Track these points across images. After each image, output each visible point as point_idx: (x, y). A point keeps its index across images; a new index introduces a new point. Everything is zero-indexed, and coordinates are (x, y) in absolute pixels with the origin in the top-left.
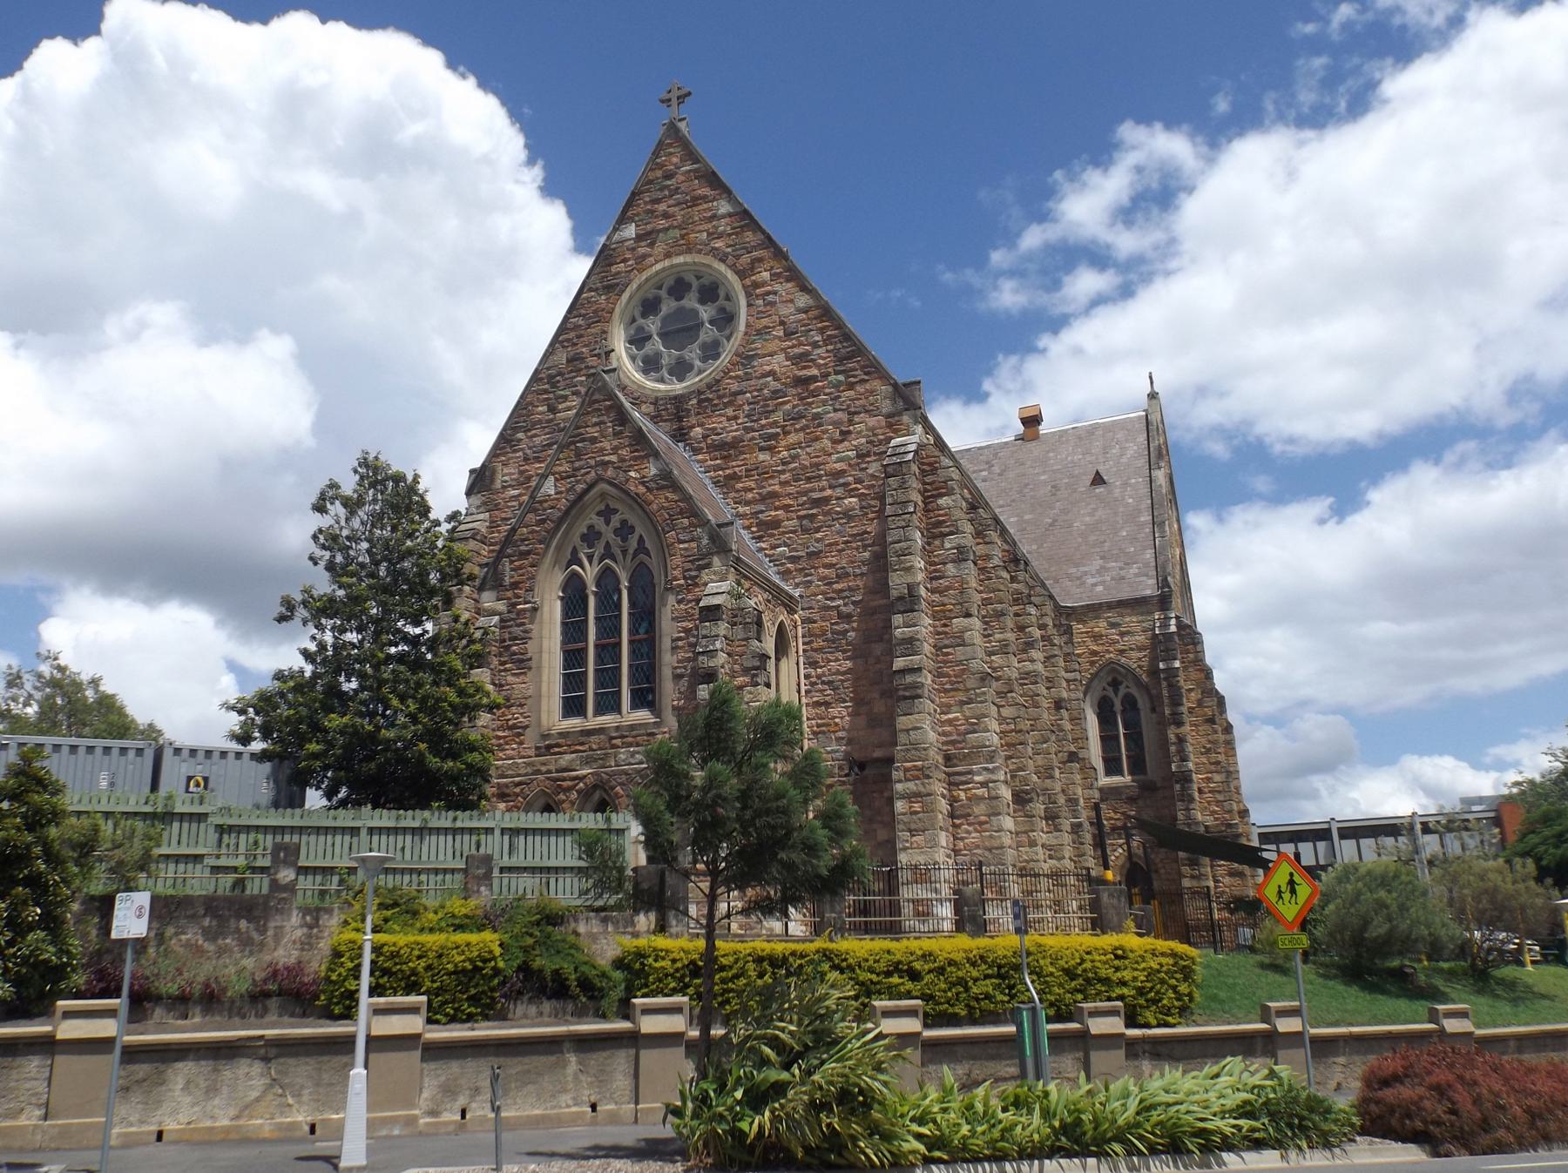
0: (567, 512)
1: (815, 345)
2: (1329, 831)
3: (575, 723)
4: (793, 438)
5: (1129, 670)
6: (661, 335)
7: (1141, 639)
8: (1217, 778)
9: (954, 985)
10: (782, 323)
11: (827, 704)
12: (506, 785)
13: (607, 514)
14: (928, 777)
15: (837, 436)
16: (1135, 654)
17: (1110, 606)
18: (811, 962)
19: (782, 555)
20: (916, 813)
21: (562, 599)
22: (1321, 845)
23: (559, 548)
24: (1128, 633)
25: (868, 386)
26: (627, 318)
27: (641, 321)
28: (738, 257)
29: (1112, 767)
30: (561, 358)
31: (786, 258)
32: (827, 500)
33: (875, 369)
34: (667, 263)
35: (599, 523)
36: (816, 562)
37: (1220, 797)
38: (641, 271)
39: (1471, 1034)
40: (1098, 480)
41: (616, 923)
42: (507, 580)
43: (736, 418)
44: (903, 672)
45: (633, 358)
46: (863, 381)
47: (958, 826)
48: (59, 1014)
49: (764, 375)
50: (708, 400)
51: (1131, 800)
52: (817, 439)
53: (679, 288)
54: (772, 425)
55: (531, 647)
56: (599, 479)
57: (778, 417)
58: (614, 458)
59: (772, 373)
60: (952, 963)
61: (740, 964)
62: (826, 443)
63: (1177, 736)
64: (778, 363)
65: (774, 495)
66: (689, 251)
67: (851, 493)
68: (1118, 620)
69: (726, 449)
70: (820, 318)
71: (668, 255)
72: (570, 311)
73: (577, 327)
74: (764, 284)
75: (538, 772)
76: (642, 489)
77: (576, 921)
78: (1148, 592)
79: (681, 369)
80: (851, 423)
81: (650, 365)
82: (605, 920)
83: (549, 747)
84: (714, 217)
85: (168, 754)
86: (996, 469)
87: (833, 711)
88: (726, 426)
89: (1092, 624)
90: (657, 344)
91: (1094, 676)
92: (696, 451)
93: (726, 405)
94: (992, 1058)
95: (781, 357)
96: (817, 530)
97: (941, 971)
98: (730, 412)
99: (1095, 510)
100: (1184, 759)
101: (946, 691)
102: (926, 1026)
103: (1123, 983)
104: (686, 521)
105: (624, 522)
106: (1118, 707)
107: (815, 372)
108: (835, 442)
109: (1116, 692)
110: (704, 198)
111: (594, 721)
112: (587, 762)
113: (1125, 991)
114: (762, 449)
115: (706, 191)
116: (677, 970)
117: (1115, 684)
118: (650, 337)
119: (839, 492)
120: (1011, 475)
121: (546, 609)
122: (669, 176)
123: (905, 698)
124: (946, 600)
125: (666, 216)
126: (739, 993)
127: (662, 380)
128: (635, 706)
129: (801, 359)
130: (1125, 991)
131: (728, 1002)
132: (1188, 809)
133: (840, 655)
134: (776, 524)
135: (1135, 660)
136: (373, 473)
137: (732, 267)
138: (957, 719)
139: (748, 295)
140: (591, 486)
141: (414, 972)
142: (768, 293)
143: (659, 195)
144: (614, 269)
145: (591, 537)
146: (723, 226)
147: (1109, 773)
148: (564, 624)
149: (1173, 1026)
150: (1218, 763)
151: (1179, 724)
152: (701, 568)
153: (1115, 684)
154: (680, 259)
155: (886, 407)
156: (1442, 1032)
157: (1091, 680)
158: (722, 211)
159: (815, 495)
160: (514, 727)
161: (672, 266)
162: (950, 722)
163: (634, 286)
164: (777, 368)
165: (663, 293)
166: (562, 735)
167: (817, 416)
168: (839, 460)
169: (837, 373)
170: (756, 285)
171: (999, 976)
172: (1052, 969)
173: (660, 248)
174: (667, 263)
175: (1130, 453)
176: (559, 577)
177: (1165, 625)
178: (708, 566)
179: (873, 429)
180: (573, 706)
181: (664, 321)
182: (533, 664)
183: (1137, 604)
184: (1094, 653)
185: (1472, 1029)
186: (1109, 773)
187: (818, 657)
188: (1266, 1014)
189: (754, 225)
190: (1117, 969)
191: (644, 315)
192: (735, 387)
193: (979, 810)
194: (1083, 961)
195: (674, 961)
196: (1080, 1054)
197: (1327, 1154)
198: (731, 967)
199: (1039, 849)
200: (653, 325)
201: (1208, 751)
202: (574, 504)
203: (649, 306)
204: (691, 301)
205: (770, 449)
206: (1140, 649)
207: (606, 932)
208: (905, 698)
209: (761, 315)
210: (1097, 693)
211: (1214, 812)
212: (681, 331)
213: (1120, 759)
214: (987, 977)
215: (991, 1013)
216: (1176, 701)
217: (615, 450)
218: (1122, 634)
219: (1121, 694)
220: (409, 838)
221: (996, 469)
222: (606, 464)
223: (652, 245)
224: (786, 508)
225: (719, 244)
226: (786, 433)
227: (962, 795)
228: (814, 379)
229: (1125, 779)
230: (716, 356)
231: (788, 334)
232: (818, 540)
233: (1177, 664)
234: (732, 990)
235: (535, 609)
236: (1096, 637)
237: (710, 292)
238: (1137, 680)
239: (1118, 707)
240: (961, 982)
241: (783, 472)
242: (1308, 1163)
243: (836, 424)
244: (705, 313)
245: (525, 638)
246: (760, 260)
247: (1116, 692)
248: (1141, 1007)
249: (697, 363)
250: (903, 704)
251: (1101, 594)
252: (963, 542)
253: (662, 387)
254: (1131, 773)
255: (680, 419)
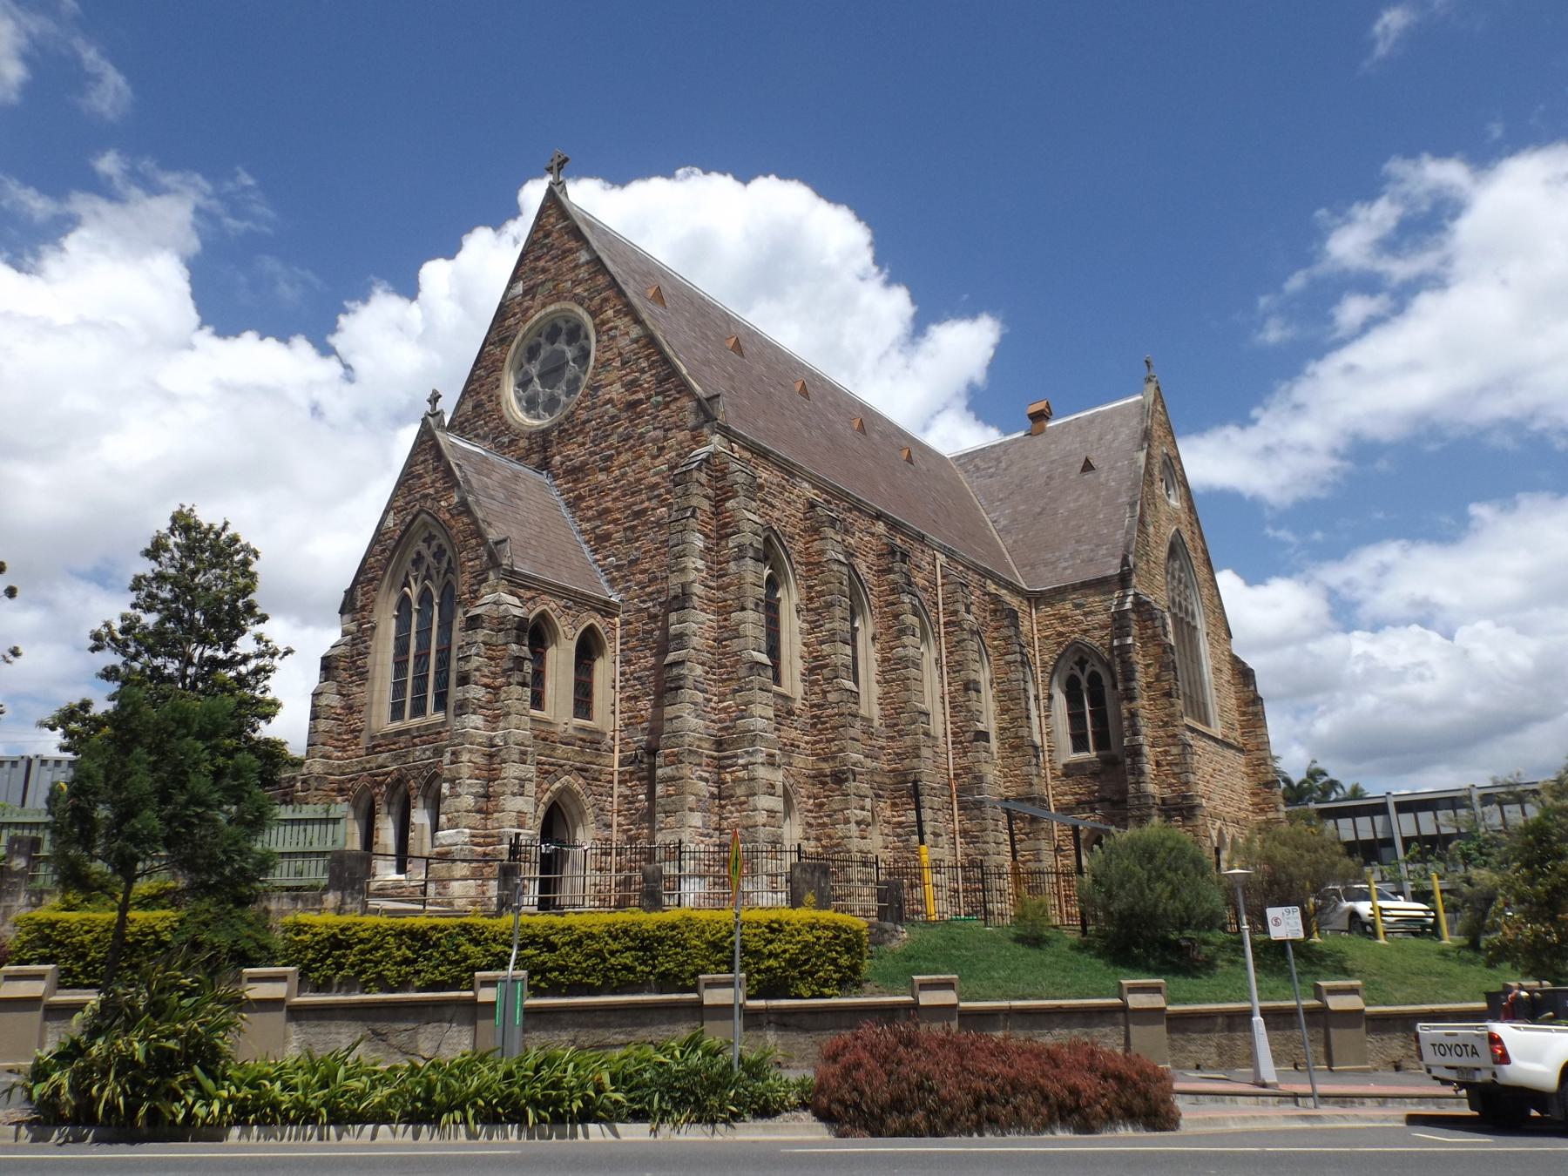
0: (398, 542)
1: (643, 371)
2: (1470, 798)
3: (397, 725)
4: (623, 458)
5: (1093, 650)
6: (540, 377)
7: (1103, 617)
8: (1174, 750)
9: (589, 956)
10: (620, 354)
11: (636, 698)
12: (343, 782)
13: (429, 540)
14: (681, 762)
15: (655, 452)
16: (1098, 633)
17: (1074, 588)
18: (450, 935)
19: (611, 563)
20: (670, 796)
21: (397, 617)
22: (1379, 819)
23: (394, 574)
24: (1091, 613)
25: (678, 404)
26: (516, 365)
27: (526, 366)
28: (591, 300)
29: (1079, 743)
30: (469, 405)
31: (625, 295)
32: (643, 512)
33: (684, 388)
34: (543, 313)
35: (421, 546)
36: (635, 569)
37: (1177, 770)
38: (525, 322)
39: (1362, 1011)
40: (1088, 466)
41: (305, 901)
42: (359, 604)
43: (584, 444)
44: (671, 665)
45: (519, 400)
46: (676, 399)
47: (723, 807)
48: (244, 979)
49: (606, 403)
50: (565, 430)
51: (1095, 775)
52: (640, 456)
53: (553, 334)
54: (609, 447)
55: (369, 660)
56: (421, 511)
57: (614, 439)
58: (431, 491)
59: (610, 401)
60: (591, 936)
61: (378, 938)
62: (647, 459)
63: (1129, 711)
64: (616, 391)
65: (607, 511)
66: (558, 300)
67: (663, 503)
68: (1081, 601)
69: (576, 472)
70: (646, 346)
71: (544, 306)
72: (475, 364)
73: (480, 377)
74: (609, 321)
75: (364, 769)
76: (448, 516)
77: (269, 900)
78: (1111, 572)
79: (552, 405)
80: (666, 439)
81: (530, 405)
82: (295, 899)
83: (375, 747)
84: (576, 266)
85: (36, 764)
86: (1003, 465)
87: (640, 705)
88: (575, 452)
89: (1058, 606)
90: (537, 385)
91: (1061, 656)
92: (555, 477)
93: (578, 433)
94: (598, 1026)
95: (618, 386)
96: (637, 539)
97: (578, 943)
98: (580, 439)
99: (1080, 495)
100: (1136, 733)
101: (724, 681)
102: (960, 1000)
103: (771, 955)
104: (474, 542)
105: (440, 546)
106: (1084, 685)
107: (641, 395)
108: (654, 457)
109: (1082, 671)
110: (571, 251)
111: (411, 722)
112: (395, 759)
113: (772, 962)
114: (601, 470)
115: (573, 244)
116: (317, 943)
117: (1081, 663)
118: (531, 380)
119: (654, 503)
120: (1014, 469)
121: (381, 628)
122: (547, 236)
123: (671, 689)
124: (727, 596)
125: (544, 270)
126: (377, 964)
127: (539, 417)
128: (437, 709)
129: (632, 386)
130: (772, 962)
131: (364, 972)
132: (1138, 783)
133: (648, 652)
134: (607, 537)
135: (1095, 640)
136: (183, 523)
137: (587, 309)
138: (730, 707)
139: (598, 332)
140: (415, 517)
141: (82, 945)
142: (611, 329)
143: (539, 253)
144: (507, 323)
145: (418, 560)
146: (583, 273)
147: (1076, 749)
148: (397, 639)
149: (830, 997)
150: (1175, 736)
151: (1132, 699)
152: (481, 582)
153: (1081, 663)
154: (551, 308)
155: (691, 421)
156: (1124, 1008)
157: (1058, 661)
158: (583, 260)
159: (636, 508)
160: (353, 731)
161: (547, 315)
162: (725, 709)
163: (520, 336)
164: (614, 396)
165: (542, 340)
166: (384, 736)
167: (642, 435)
168: (656, 474)
169: (657, 394)
170: (603, 323)
171: (644, 949)
172: (695, 942)
173: (539, 299)
174: (543, 313)
175: (1123, 437)
176: (394, 598)
177: (1121, 603)
178: (486, 580)
179: (680, 443)
180: (397, 712)
181: (543, 363)
182: (369, 675)
183: (1099, 585)
184: (1061, 634)
185: (1163, 1005)
186: (1076, 749)
187: (632, 655)
188: (1318, 992)
189: (604, 270)
190: (771, 942)
191: (529, 360)
192: (584, 417)
193: (740, 791)
194: (731, 933)
195: (315, 935)
196: (1321, 1035)
197: (708, 1129)
198: (370, 941)
199: (853, 826)
200: (534, 369)
201: (1166, 724)
202: (404, 533)
203: (532, 353)
204: (561, 345)
205: (606, 469)
206: (1102, 628)
207: (295, 908)
208: (671, 689)
209: (608, 348)
210: (1065, 675)
211: (1171, 785)
212: (552, 373)
213: (1086, 735)
214: (628, 949)
215: (631, 983)
216: (1129, 676)
217: (433, 482)
218: (1086, 614)
219: (1087, 673)
220: (317, 827)
221: (1003, 465)
222: (425, 496)
223: (533, 299)
224: (615, 521)
225: (579, 290)
226: (619, 454)
227: (728, 778)
228: (640, 402)
229: (1091, 755)
230: (577, 389)
231: (624, 364)
232: (637, 549)
233: (1130, 641)
234: (370, 961)
235: (373, 628)
236: (1063, 619)
237: (575, 333)
238: (1101, 660)
239: (1084, 685)
240: (599, 954)
241: (614, 489)
242: (681, 1138)
243: (654, 441)
244: (570, 353)
245: (364, 654)
246: (606, 300)
247: (1082, 671)
248: (793, 978)
249: (563, 398)
250: (668, 695)
251: (1070, 576)
252: (742, 540)
253: (536, 422)
254: (1097, 748)
255: (545, 450)
